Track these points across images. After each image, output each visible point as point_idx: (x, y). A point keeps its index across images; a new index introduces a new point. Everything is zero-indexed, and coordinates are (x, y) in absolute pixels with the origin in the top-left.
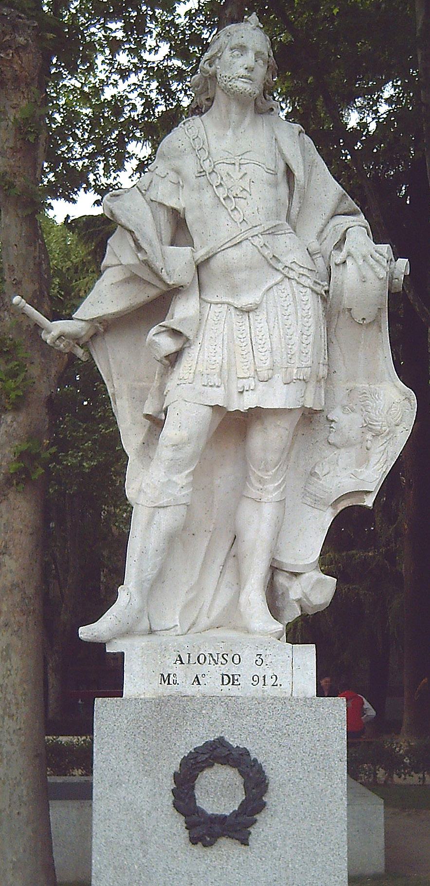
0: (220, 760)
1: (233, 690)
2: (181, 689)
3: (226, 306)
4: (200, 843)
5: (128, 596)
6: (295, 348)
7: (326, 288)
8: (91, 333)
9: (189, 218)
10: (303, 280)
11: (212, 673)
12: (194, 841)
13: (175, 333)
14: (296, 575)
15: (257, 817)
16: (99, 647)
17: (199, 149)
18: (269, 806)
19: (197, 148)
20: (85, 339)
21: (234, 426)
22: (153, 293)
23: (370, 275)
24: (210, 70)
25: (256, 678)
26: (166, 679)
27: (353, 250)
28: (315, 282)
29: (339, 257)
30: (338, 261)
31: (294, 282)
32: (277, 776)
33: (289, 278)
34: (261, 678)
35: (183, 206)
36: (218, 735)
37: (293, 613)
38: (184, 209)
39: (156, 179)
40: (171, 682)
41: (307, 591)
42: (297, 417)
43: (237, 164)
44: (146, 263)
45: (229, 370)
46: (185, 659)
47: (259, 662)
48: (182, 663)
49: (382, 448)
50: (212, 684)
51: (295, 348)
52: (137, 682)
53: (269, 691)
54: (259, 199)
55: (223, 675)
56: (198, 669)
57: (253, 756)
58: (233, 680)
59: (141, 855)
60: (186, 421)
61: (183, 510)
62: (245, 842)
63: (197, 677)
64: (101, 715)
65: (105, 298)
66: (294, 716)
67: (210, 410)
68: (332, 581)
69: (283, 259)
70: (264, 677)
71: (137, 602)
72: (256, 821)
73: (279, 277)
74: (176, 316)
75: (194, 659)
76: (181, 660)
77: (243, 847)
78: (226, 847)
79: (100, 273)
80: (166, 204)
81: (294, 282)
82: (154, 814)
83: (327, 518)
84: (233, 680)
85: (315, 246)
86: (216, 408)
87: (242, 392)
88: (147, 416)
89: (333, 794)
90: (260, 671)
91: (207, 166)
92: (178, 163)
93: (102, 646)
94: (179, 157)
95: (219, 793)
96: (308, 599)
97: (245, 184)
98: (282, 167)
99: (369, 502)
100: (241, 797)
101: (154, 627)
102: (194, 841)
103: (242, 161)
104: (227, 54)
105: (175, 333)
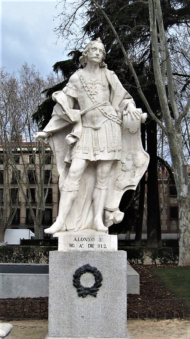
1: (91, 249)
2: (76, 249)
7: (121, 122)
8: (48, 136)
9: (79, 101)
10: (114, 120)
12: (80, 295)
13: (74, 137)
14: (111, 212)
18: (103, 285)
22: (64, 125)
24: (86, 55)
25: (99, 245)
26: (71, 245)
27: (129, 110)
31: (111, 121)
33: (110, 119)
34: (101, 246)
36: (87, 263)
37: (110, 224)
40: (73, 246)
46: (77, 240)
48: (76, 241)
49: (139, 172)
50: (86, 248)
52: (62, 247)
54: (101, 94)
55: (89, 244)
56: (81, 243)
58: (92, 246)
60: (78, 165)
62: (95, 296)
63: (81, 245)
67: (85, 161)
72: (98, 290)
78: (89, 298)
83: (123, 192)
84: (92, 246)
85: (118, 109)
90: (100, 243)
92: (75, 84)
97: (96, 90)
99: (135, 188)
100: (94, 282)
104: (91, 50)
105: (74, 137)
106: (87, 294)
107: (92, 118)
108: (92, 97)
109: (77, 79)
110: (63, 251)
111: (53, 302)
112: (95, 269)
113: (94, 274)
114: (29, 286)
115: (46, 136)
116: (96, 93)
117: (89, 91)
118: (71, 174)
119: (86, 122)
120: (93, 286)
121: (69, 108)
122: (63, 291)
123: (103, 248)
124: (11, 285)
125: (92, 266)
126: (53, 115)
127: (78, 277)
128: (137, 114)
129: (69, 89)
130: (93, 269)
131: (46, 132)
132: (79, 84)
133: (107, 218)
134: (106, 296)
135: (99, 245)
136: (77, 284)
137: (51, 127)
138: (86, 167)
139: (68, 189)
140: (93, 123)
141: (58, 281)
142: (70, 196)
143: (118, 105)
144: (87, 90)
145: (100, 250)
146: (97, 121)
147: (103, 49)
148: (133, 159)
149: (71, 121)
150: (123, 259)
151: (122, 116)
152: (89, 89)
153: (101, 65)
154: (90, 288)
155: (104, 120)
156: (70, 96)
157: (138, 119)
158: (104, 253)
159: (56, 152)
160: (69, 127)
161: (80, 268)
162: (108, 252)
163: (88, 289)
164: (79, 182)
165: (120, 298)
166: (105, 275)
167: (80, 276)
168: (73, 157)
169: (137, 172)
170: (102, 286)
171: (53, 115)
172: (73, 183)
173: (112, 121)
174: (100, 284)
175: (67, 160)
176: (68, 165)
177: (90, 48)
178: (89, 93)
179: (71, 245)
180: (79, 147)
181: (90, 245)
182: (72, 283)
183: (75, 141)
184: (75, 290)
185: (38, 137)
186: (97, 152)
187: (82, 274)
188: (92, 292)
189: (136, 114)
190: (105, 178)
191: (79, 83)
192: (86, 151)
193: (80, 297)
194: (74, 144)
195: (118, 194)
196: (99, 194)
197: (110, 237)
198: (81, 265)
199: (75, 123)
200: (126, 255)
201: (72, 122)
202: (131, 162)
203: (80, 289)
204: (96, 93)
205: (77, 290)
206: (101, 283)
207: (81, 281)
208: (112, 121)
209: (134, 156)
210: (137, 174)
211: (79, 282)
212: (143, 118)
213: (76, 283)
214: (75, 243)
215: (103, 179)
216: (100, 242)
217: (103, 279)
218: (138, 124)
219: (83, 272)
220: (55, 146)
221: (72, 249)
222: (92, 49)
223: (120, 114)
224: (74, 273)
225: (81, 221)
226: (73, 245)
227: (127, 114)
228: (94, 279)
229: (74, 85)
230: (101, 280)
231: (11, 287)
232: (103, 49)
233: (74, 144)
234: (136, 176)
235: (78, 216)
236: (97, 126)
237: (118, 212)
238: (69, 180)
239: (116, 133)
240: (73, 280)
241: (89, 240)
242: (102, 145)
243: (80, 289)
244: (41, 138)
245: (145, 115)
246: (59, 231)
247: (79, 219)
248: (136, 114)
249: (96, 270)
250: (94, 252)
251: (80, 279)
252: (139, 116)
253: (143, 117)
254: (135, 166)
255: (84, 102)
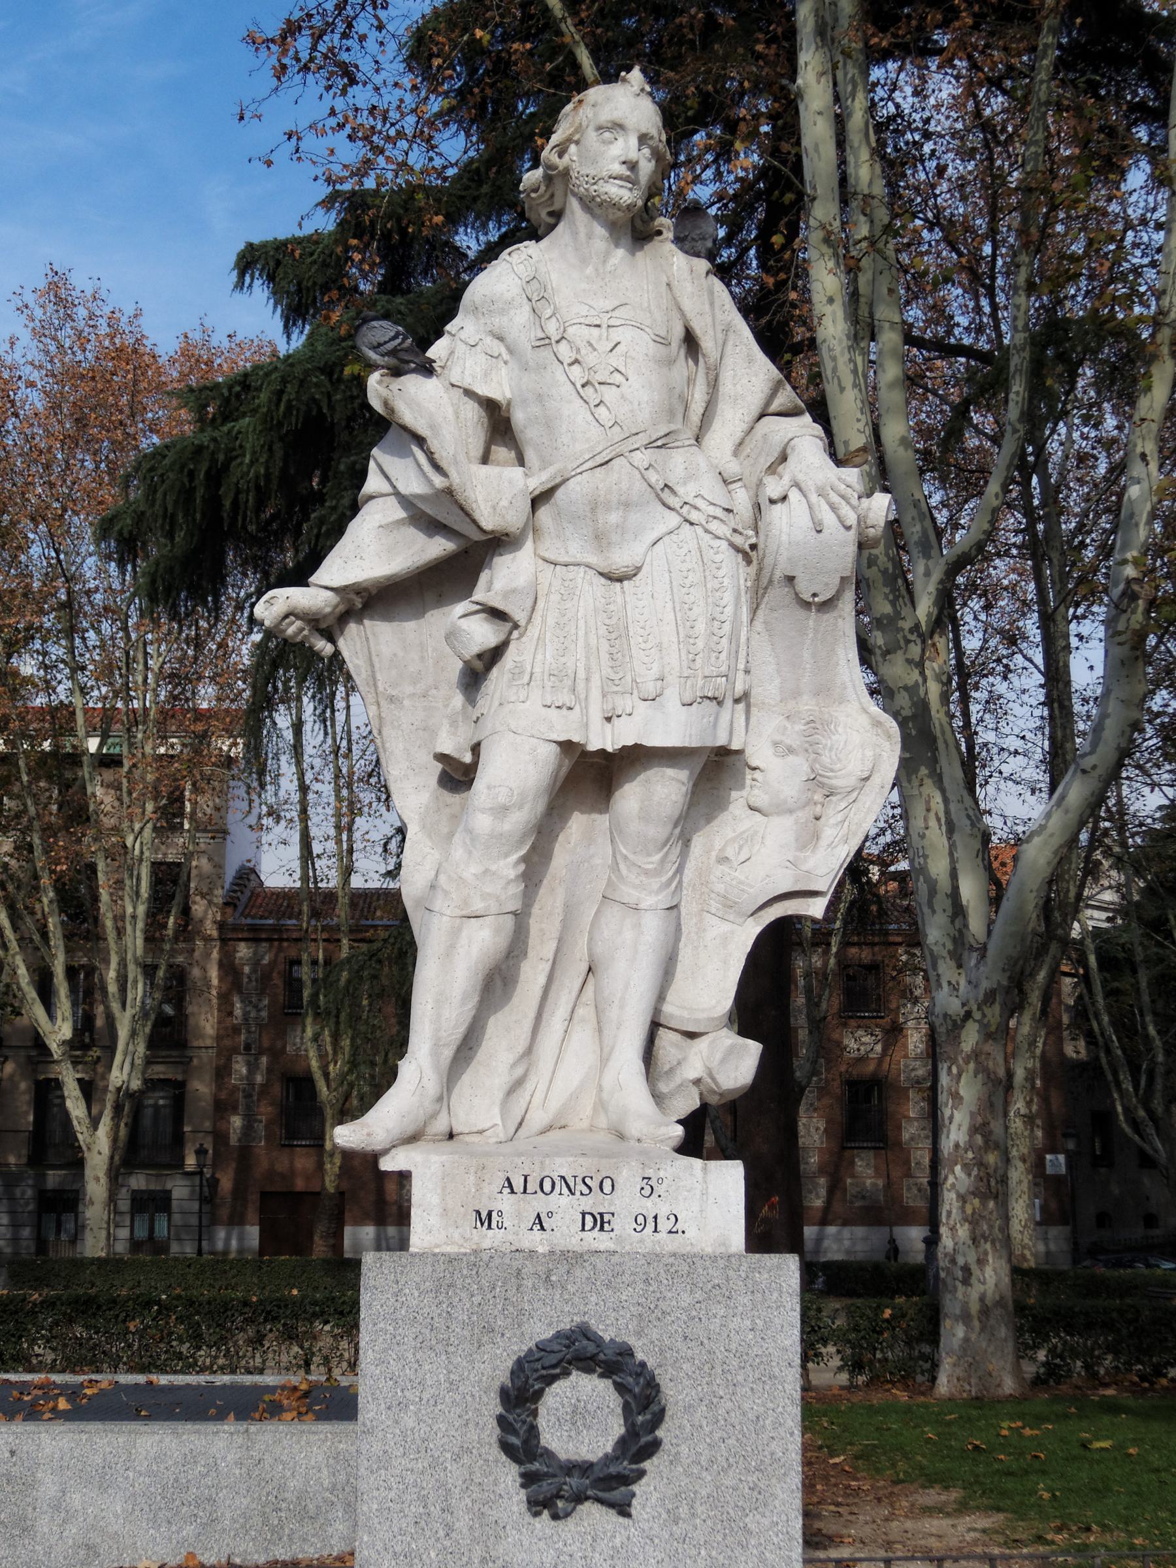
0: (580, 1365)
1: (597, 1240)
2: (511, 1238)
3: (582, 569)
4: (546, 1512)
5: (418, 1070)
6: (700, 644)
7: (753, 540)
8: (342, 608)
9: (519, 417)
10: (714, 526)
11: (565, 1209)
12: (537, 1505)
13: (496, 614)
14: (691, 1035)
15: (646, 1465)
16: (364, 1163)
17: (538, 297)
18: (666, 1445)
19: (535, 298)
20: (330, 621)
21: (590, 776)
22: (439, 547)
23: (829, 518)
24: (561, 163)
25: (640, 1219)
26: (486, 1219)
27: (801, 477)
28: (735, 531)
29: (773, 488)
30: (775, 495)
31: (699, 530)
32: (680, 1393)
33: (692, 524)
34: (650, 1221)
35: (509, 395)
36: (577, 1319)
37: (688, 1103)
38: (509, 404)
39: (461, 349)
40: (494, 1225)
41: (714, 1064)
42: (699, 763)
43: (604, 326)
44: (449, 492)
45: (587, 680)
46: (518, 1184)
47: (647, 1191)
48: (513, 1192)
49: (840, 817)
50: (567, 1232)
51: (700, 644)
52: (429, 1227)
53: (669, 1244)
54: (639, 387)
55: (583, 1214)
56: (539, 1204)
57: (640, 1356)
59: (441, 1533)
60: (517, 769)
61: (509, 921)
62: (623, 1509)
63: (538, 1216)
64: (372, 1283)
65: (372, 547)
66: (710, 1286)
67: (555, 748)
68: (753, 1049)
69: (680, 490)
70: (656, 1217)
71: (432, 1086)
72: (642, 1473)
73: (673, 520)
74: (498, 585)
75: (533, 1186)
76: (510, 1186)
77: (621, 1519)
78: (593, 1516)
79: (355, 508)
80: (480, 392)
81: (699, 530)
82: (709, 1522)
83: (753, 929)
84: (601, 1222)
85: (733, 467)
86: (567, 746)
87: (609, 719)
88: (442, 758)
89: (777, 1424)
90: (649, 1207)
91: (552, 328)
92: (497, 322)
93: (373, 1158)
94: (502, 312)
95: (580, 1419)
96: (713, 1079)
97: (615, 360)
98: (678, 332)
99: (816, 909)
100: (617, 1429)
101: (457, 1129)
102: (537, 1505)
103: (612, 322)
104: (591, 136)
105: (496, 614)
106: (579, 1498)
107: (593, 510)
108: (593, 399)
109: (508, 296)
110: (437, 1250)
111: (379, 1546)
112: (620, 1354)
113: (615, 1383)
114: (134, 1495)
115: (328, 610)
116: (618, 378)
117: (576, 361)
118: (483, 822)
119: (558, 537)
120: (609, 1449)
121: (461, 457)
122: (441, 1485)
123: (663, 1235)
124: (30, 1485)
125: (607, 1338)
126: (371, 497)
127: (527, 1400)
128: (843, 497)
129: (461, 349)
130: (609, 1354)
131: (326, 588)
132: (519, 322)
133: (666, 1067)
134: (683, 1511)
135: (640, 1219)
136: (525, 1442)
137: (358, 561)
138: (559, 784)
139: (466, 902)
140: (600, 539)
141: (410, 1422)
142: (481, 942)
143: (729, 447)
144: (567, 361)
145: (649, 1245)
146: (621, 528)
147: (656, 135)
148: (811, 748)
149: (474, 521)
150: (775, 1295)
151: (758, 507)
152: (578, 351)
153: (638, 223)
154: (591, 1465)
155: (661, 529)
156: (469, 393)
157: (848, 528)
158: (671, 1260)
159: (383, 703)
160: (462, 560)
161: (541, 1347)
162: (692, 1259)
163: (583, 1468)
164: (522, 867)
165: (766, 1522)
166: (676, 1393)
167: (539, 1394)
168: (488, 725)
169: (832, 821)
170: (660, 1453)
171: (371, 497)
172: (494, 868)
173: (707, 531)
174: (649, 1438)
175: (452, 744)
176: (458, 776)
177: (584, 124)
178: (576, 372)
179: (486, 1219)
180: (522, 673)
181: (589, 1218)
182: (492, 1432)
183: (502, 637)
184: (509, 1474)
185: (286, 616)
186: (624, 703)
187: (550, 1380)
188: (611, 1483)
189: (835, 498)
190: (665, 845)
191: (521, 316)
192: (565, 698)
193: (536, 1514)
194: (493, 656)
195: (725, 940)
196: (628, 935)
197: (705, 1169)
198: (541, 1330)
199: (498, 543)
200: (797, 1275)
201: (477, 536)
202: (800, 765)
203: (536, 1466)
204: (618, 378)
205: (523, 1475)
206: (660, 1433)
207: (542, 1422)
208: (707, 531)
209: (816, 727)
210: (829, 833)
211: (533, 1431)
212: (869, 523)
213: (515, 1432)
214: (506, 1203)
215: (649, 855)
216: (649, 1203)
217: (668, 1413)
218: (841, 553)
219: (558, 1371)
220: (377, 666)
221: (490, 1239)
222: (599, 128)
223: (742, 499)
224: (503, 1376)
225: (529, 1086)
226: (494, 1214)
227: (784, 498)
228: (619, 1410)
229: (492, 334)
230: (659, 1418)
231: (28, 1500)
232: (656, 135)
233: (493, 656)
234: (824, 842)
235: (511, 1058)
236: (620, 559)
237: (729, 1038)
238: (470, 853)
239: (728, 597)
240: (501, 1420)
241: (586, 1191)
242: (645, 668)
243: (536, 1466)
244: (297, 617)
245: (880, 506)
246: (413, 1139)
247: (519, 1071)
248: (835, 498)
249: (628, 1359)
250: (615, 1259)
251: (535, 1413)
252: (853, 508)
253: (871, 515)
254: (822, 785)
255: (549, 424)
